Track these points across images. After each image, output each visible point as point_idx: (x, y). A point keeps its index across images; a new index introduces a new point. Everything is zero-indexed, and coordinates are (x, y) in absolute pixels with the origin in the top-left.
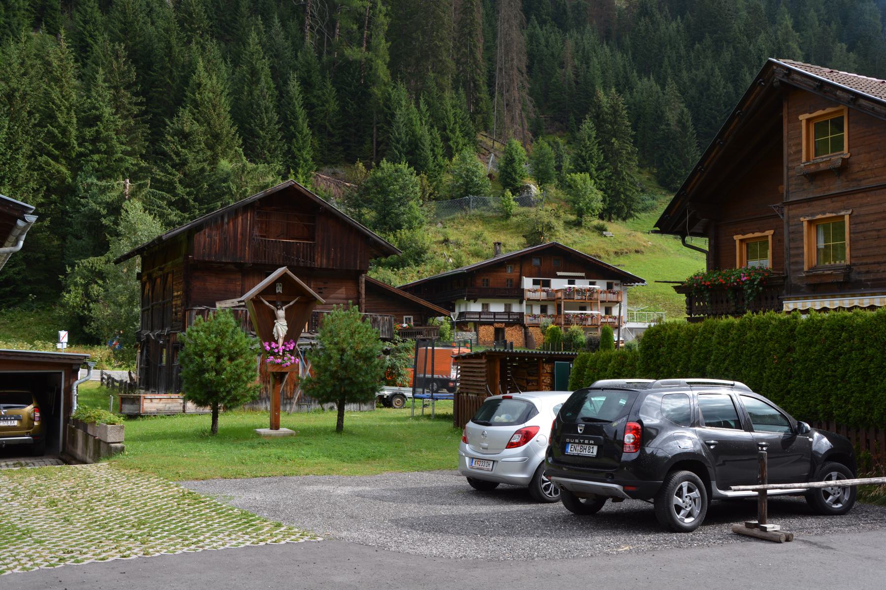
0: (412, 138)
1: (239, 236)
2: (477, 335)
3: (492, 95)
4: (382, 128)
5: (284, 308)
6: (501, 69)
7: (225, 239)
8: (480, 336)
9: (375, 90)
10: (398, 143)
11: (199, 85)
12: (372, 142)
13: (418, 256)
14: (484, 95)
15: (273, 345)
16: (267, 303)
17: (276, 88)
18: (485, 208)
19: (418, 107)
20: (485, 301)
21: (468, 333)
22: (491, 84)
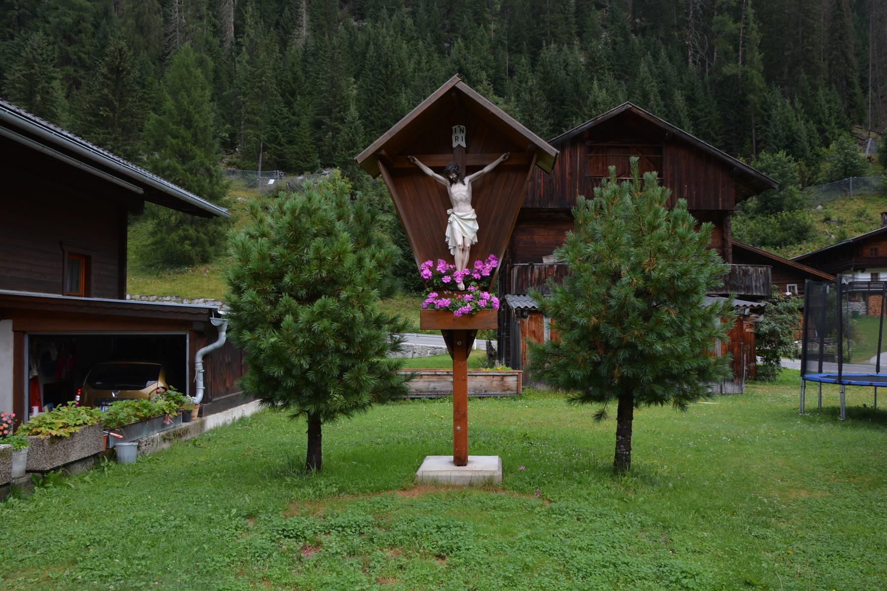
0: (789, 133)
1: (567, 176)
2: (867, 305)
3: (865, 91)
4: (760, 128)
5: (467, 180)
6: (874, 66)
7: (551, 181)
8: (871, 305)
9: (751, 96)
10: (775, 138)
11: (595, 104)
12: (752, 142)
13: (802, 234)
14: (858, 90)
15: (441, 267)
16: (430, 172)
17: (665, 106)
18: (866, 188)
19: (792, 103)
20: (875, 271)
21: (857, 303)
22: (863, 80)
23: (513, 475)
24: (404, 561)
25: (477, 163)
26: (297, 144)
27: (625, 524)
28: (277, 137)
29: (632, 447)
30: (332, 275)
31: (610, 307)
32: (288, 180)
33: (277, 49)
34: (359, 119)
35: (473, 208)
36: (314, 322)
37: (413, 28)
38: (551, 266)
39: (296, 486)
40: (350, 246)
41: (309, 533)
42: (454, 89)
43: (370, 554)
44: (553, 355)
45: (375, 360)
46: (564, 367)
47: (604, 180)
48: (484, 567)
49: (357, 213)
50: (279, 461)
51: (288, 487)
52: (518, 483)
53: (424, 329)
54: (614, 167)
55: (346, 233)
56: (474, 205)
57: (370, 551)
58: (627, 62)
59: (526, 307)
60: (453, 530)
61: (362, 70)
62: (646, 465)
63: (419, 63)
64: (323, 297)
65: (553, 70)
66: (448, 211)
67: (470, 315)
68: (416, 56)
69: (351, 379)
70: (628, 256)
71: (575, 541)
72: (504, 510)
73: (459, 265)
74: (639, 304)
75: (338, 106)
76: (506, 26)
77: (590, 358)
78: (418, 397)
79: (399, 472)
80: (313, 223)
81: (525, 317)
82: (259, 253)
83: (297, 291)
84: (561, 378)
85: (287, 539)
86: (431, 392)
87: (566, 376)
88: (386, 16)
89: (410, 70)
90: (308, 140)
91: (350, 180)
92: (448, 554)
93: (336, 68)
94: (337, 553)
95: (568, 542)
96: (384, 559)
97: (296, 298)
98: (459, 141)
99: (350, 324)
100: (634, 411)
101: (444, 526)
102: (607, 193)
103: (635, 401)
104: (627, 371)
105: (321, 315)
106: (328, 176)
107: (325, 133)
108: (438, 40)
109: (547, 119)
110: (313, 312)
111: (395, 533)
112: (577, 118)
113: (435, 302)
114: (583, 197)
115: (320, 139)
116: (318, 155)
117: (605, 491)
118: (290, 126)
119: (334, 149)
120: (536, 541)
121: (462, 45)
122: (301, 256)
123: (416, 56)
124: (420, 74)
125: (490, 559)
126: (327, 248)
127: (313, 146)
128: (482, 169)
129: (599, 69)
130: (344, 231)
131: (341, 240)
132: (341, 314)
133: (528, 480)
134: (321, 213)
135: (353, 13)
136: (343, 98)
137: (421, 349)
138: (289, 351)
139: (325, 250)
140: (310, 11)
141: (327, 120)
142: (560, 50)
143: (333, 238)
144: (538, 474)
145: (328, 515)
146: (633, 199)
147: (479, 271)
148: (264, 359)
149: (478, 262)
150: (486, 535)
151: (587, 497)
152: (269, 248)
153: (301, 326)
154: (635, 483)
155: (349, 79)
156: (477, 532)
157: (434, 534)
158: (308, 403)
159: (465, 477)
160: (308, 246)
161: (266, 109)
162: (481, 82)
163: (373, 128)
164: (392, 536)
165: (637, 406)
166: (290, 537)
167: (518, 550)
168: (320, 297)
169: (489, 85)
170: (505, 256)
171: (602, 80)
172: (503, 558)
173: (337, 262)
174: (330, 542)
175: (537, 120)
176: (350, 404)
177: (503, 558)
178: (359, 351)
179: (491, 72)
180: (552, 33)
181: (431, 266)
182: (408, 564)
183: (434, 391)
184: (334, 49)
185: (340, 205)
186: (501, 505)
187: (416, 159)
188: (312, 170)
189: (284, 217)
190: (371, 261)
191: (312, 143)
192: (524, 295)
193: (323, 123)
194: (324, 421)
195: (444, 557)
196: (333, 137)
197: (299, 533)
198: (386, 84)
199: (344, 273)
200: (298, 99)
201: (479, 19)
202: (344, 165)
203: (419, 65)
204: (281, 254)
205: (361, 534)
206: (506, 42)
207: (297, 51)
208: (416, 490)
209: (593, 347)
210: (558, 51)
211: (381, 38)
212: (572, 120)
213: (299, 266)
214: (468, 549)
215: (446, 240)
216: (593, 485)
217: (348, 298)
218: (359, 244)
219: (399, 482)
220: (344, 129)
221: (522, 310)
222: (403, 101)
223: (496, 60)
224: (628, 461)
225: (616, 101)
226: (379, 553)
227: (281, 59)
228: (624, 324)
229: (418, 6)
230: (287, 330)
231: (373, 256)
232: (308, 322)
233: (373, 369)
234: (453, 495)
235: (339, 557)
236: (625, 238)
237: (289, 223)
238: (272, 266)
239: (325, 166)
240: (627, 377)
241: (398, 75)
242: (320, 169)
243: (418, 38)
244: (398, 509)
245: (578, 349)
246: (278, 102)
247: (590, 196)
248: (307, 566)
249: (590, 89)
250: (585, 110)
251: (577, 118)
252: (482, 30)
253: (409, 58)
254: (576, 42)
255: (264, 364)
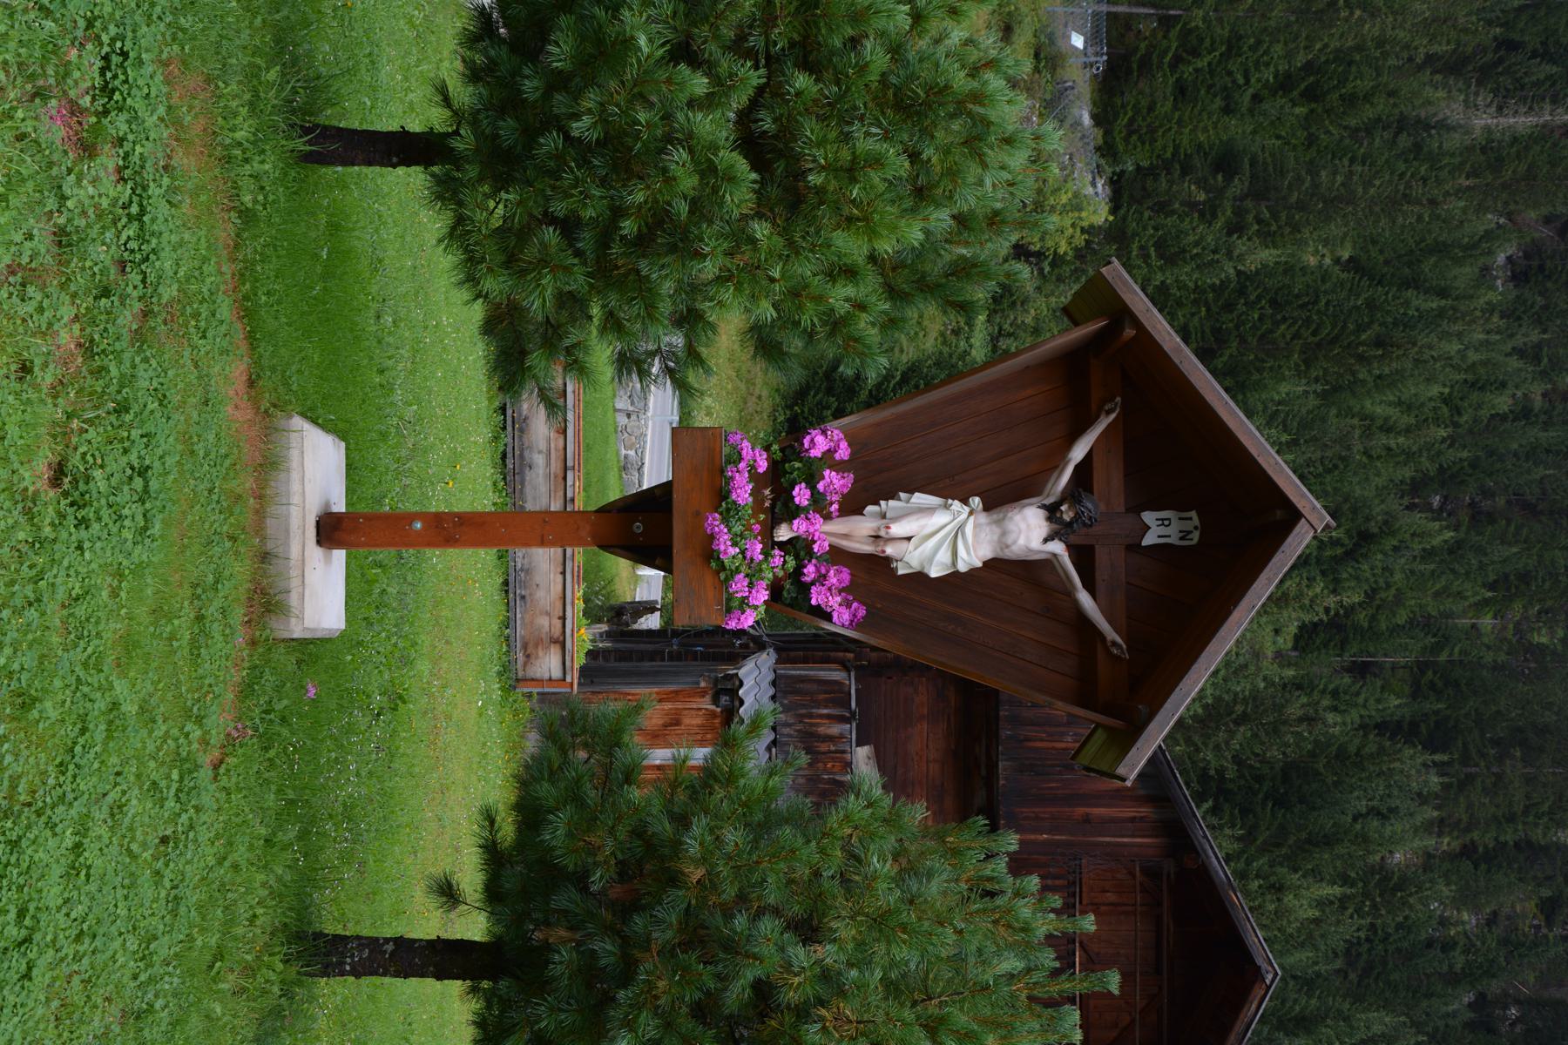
1: (1081, 810)
5: (1057, 547)
11: (1278, 889)
15: (834, 482)
16: (1078, 453)
23: (292, 667)
24: (47, 378)
25: (1102, 575)
26: (1175, 108)
27: (148, 966)
28: (1195, 53)
29: (365, 980)
30: (812, 199)
31: (728, 916)
32: (1080, 81)
33: (1436, 48)
34: (1239, 273)
35: (985, 563)
36: (691, 151)
37: (1485, 413)
38: (848, 766)
39: (256, 95)
40: (886, 247)
41: (119, 124)
42: (1293, 516)
43: (63, 286)
44: (608, 769)
45: (595, 311)
46: (575, 797)
47: (1056, 901)
48: (29, 591)
49: (975, 265)
50: (324, 52)
51: (252, 75)
52: (269, 679)
53: (681, 435)
54: (1093, 928)
55: (920, 236)
56: (992, 565)
57: (73, 288)
58: (1395, 976)
59: (742, 702)
60: (138, 509)
61: (1371, 279)
62: (315, 1020)
63: (1387, 429)
64: (754, 176)
65: (1369, 779)
66: (977, 499)
67: (709, 554)
68: (1407, 420)
69: (544, 246)
70: (861, 961)
71: (103, 831)
72: (194, 645)
73: (837, 526)
74: (737, 993)
75: (1275, 216)
76: (1489, 657)
77: (596, 864)
78: (507, 422)
79: (299, 371)
80: (947, 151)
81: (715, 701)
82: (870, 7)
83: (771, 109)
84: (545, 790)
85: (99, 64)
86: (522, 456)
87: (552, 803)
88: (1519, 341)
89: (1368, 403)
90: (1185, 142)
91: (1076, 249)
92: (66, 494)
93: (1377, 209)
94: (64, 198)
95: (100, 814)
96: (50, 325)
97: (754, 104)
98: (1158, 528)
99: (685, 247)
100: (459, 982)
101: (146, 486)
102: (1025, 910)
103: (485, 984)
104: (563, 960)
105: (707, 170)
106: (1090, 190)
107: (1202, 184)
108: (1448, 478)
109: (1237, 759)
110: (714, 148)
111: (127, 356)
112: (1239, 839)
113: (742, 465)
114: (1014, 848)
115: (1186, 170)
116: (1145, 164)
117: (242, 911)
118: (1225, 88)
119: (1162, 208)
120: (103, 727)
121: (1436, 541)
122: (862, 118)
123: (1407, 420)
124: (1357, 433)
125: (51, 607)
126: (882, 187)
127: (1170, 150)
128: (1085, 586)
129: (1373, 900)
130: (927, 232)
131: (903, 222)
132: (710, 222)
133: (278, 706)
134: (973, 170)
135: (1533, 251)
136: (1296, 229)
137: (637, 433)
138: (613, 85)
139: (877, 180)
140: (1543, 135)
141: (1238, 186)
142: (1422, 799)
143: (908, 203)
144: (293, 734)
145: (172, 178)
146: (1011, 977)
147: (821, 578)
148: (593, 17)
149: (846, 576)
150: (123, 595)
151: (227, 864)
152: (882, 34)
153: (680, 116)
154: (265, 992)
155: (1348, 245)
156: (132, 572)
157: (125, 459)
158: (478, 134)
159: (287, 544)
160: (886, 137)
161: (1272, 23)
162: (1334, 592)
163: (1215, 309)
164: (118, 346)
165: (474, 990)
166: (103, 71)
167: (78, 679)
168: (755, 167)
169: (1327, 610)
170: (874, 649)
171: (1343, 908)
172: (55, 639)
173: (846, 211)
174: (95, 181)
175: (1232, 734)
176: (476, 244)
177: (55, 639)
178: (617, 268)
179: (1362, 617)
180: (1470, 778)
181: (837, 456)
182: (36, 387)
183: (524, 465)
184: (1433, 202)
185: (995, 220)
186: (208, 636)
187: (1113, 416)
188: (1107, 150)
189: (962, 74)
190: (847, 300)
191: (1176, 148)
192: (773, 698)
193: (1229, 179)
194: (433, 175)
195: (59, 486)
196: (1192, 205)
197: (117, 96)
198: (1334, 341)
199: (818, 232)
200: (1298, 110)
201: (1506, 587)
202: (1116, 236)
203: (1381, 428)
204: (867, 65)
205: (122, 265)
206: (1443, 657)
207: (1429, 103)
208: (250, 414)
209: (625, 871)
210: (1419, 794)
211: (1457, 327)
212: (1233, 826)
213: (836, 113)
214: (80, 548)
215: (902, 495)
216: (261, 877)
217: (753, 241)
218: (894, 269)
219: (273, 369)
220: (1211, 234)
221: (733, 693)
222: (1284, 388)
223: (1395, 630)
224: (326, 971)
225: (1283, 943)
226: (67, 312)
227: (1410, 59)
228: (684, 952)
229: (1546, 426)
230: (669, 81)
231: (861, 306)
232: (690, 135)
233: (572, 304)
234: (237, 510)
235: (51, 203)
236: (906, 954)
237: (947, 87)
238: (837, 42)
239: (1116, 183)
240: (547, 962)
241: (1353, 374)
242: (1109, 170)
243: (1456, 425)
244: (196, 366)
245: (622, 833)
246: (1289, 56)
247: (1019, 866)
248: (20, 114)
249: (1317, 875)
250: (1261, 863)
251: (1239, 839)
252: (1476, 594)
253: (1400, 403)
254: (1446, 843)
255: (582, 18)
